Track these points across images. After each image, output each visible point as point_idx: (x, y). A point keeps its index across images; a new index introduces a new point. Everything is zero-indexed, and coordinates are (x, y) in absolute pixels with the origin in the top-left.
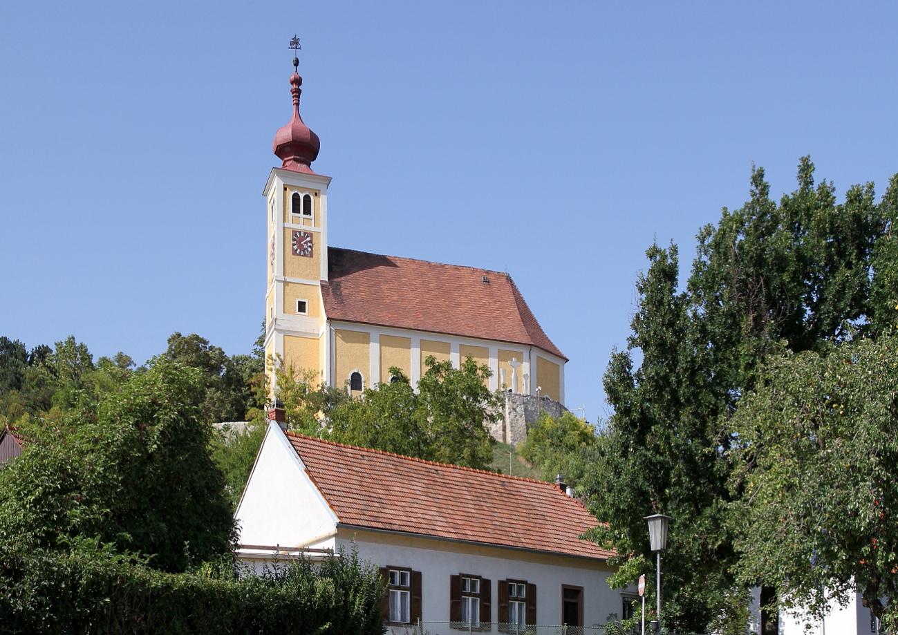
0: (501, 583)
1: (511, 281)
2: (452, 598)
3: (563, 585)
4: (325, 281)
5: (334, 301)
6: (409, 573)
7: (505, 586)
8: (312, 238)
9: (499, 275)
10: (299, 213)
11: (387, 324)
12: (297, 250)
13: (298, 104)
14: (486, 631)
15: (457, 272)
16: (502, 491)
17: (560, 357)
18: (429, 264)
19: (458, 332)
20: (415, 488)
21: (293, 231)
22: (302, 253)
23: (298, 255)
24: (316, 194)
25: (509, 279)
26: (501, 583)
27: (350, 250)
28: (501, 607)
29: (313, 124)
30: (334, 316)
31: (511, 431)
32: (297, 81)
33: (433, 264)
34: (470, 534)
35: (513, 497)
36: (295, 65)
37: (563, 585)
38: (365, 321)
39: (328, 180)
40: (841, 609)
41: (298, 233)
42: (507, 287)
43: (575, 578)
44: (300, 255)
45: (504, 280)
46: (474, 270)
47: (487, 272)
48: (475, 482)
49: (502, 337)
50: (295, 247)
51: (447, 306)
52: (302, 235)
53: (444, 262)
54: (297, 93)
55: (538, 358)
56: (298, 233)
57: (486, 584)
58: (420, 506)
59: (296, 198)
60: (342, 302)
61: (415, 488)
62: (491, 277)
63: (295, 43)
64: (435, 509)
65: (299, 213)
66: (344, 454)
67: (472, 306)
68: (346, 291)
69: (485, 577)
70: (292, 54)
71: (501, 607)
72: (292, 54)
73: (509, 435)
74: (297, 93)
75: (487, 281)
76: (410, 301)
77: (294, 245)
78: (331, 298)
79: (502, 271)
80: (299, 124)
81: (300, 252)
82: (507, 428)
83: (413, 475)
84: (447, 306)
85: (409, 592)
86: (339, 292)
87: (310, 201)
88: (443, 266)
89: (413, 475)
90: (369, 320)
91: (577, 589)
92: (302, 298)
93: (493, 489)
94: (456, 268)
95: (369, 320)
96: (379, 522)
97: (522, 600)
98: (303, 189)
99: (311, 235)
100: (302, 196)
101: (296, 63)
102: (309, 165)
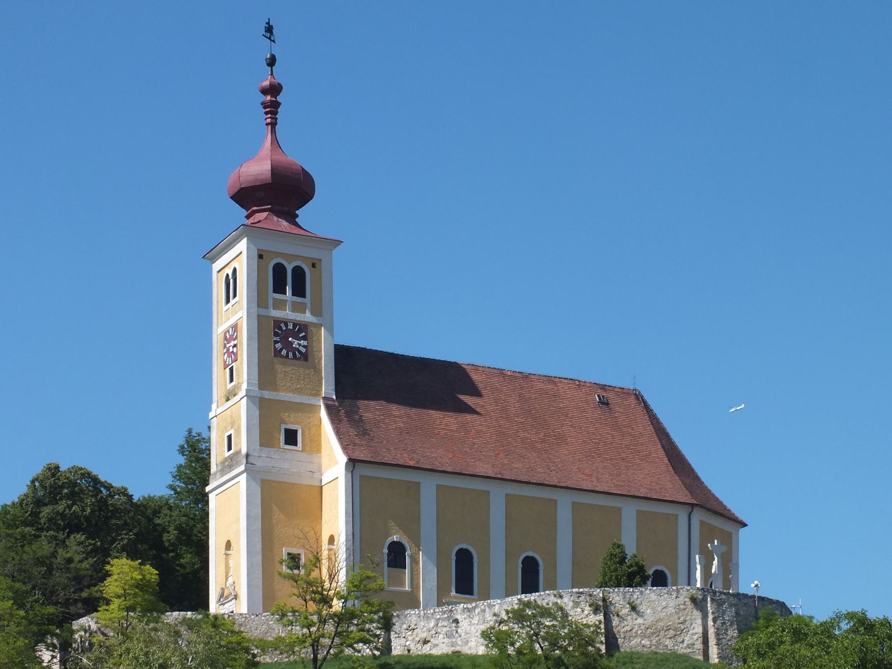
1: (645, 402)
3: (305, 298)
4: (332, 399)
5: (352, 432)
8: (282, 322)
9: (624, 392)
11: (450, 469)
12: (281, 350)
13: (273, 125)
15: (550, 386)
17: (722, 515)
18: (501, 372)
19: (569, 484)
21: (274, 321)
22: (291, 354)
23: (282, 356)
24: (314, 265)
25: (639, 397)
27: (364, 349)
31: (718, 644)
32: (274, 90)
33: (509, 373)
36: (268, 65)
37: (305, 298)
38: (411, 463)
41: (282, 325)
42: (640, 409)
45: (632, 399)
46: (580, 385)
47: (603, 387)
49: (643, 492)
50: (279, 346)
51: (543, 441)
52: (291, 327)
53: (527, 370)
54: (272, 108)
55: (702, 523)
56: (282, 325)
59: (279, 271)
62: (610, 396)
67: (584, 442)
73: (714, 651)
74: (272, 108)
75: (604, 403)
76: (479, 432)
77: (276, 342)
78: (345, 426)
79: (628, 385)
80: (279, 157)
81: (287, 354)
82: (710, 640)
84: (543, 441)
86: (357, 417)
88: (526, 377)
90: (418, 462)
94: (549, 379)
95: (418, 462)
98: (291, 257)
100: (289, 269)
101: (272, 62)
102: (292, 218)
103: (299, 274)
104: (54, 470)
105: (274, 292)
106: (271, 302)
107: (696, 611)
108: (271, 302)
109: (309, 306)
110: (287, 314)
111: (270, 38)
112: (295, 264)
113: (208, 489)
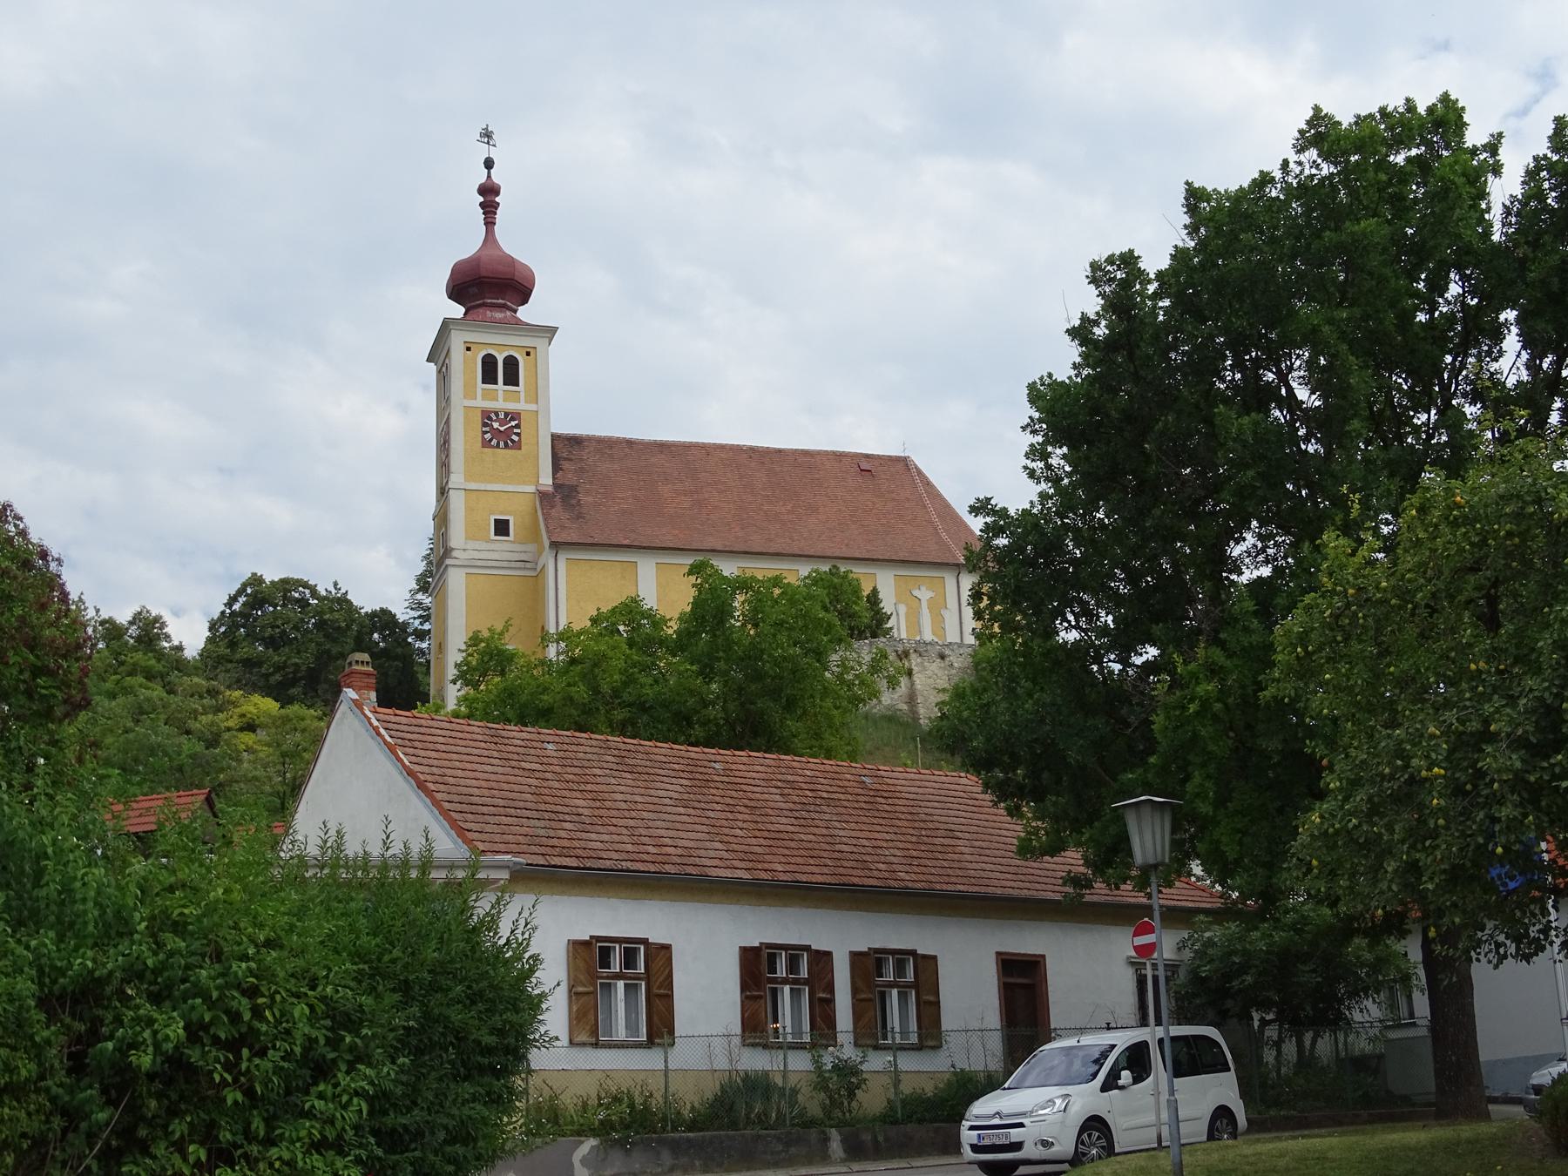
0: (856, 957)
2: (744, 987)
3: (998, 954)
6: (642, 948)
7: (867, 964)
8: (491, 412)
10: (496, 383)
12: (491, 440)
14: (933, 1048)
16: (860, 791)
19: (811, 552)
20: (661, 793)
22: (502, 444)
23: (493, 447)
24: (528, 354)
26: (856, 957)
28: (747, 997)
29: (514, 242)
30: (563, 537)
34: (780, 870)
35: (883, 801)
37: (998, 954)
38: (626, 542)
39: (550, 332)
40: (502, 528)
43: (1026, 940)
44: (498, 446)
45: (901, 465)
48: (801, 779)
49: (902, 555)
50: (488, 436)
51: (789, 512)
57: (822, 960)
58: (669, 825)
60: (580, 516)
61: (661, 793)
63: (487, 135)
64: (704, 828)
65: (496, 383)
66: (507, 741)
68: (590, 499)
69: (656, 938)
70: (483, 151)
71: (747, 997)
72: (483, 151)
81: (498, 443)
83: (661, 772)
84: (789, 512)
85: (643, 983)
86: (574, 502)
87: (518, 365)
89: (661, 772)
91: (1034, 959)
92: (501, 513)
93: (839, 790)
96: (571, 857)
97: (908, 986)
99: (513, 416)
103: (511, 364)
104: (256, 580)
105: (484, 382)
106: (479, 392)
107: (943, 683)
108: (479, 392)
109: (522, 395)
110: (501, 404)
111: (488, 143)
112: (506, 354)
113: (1525, 356)
